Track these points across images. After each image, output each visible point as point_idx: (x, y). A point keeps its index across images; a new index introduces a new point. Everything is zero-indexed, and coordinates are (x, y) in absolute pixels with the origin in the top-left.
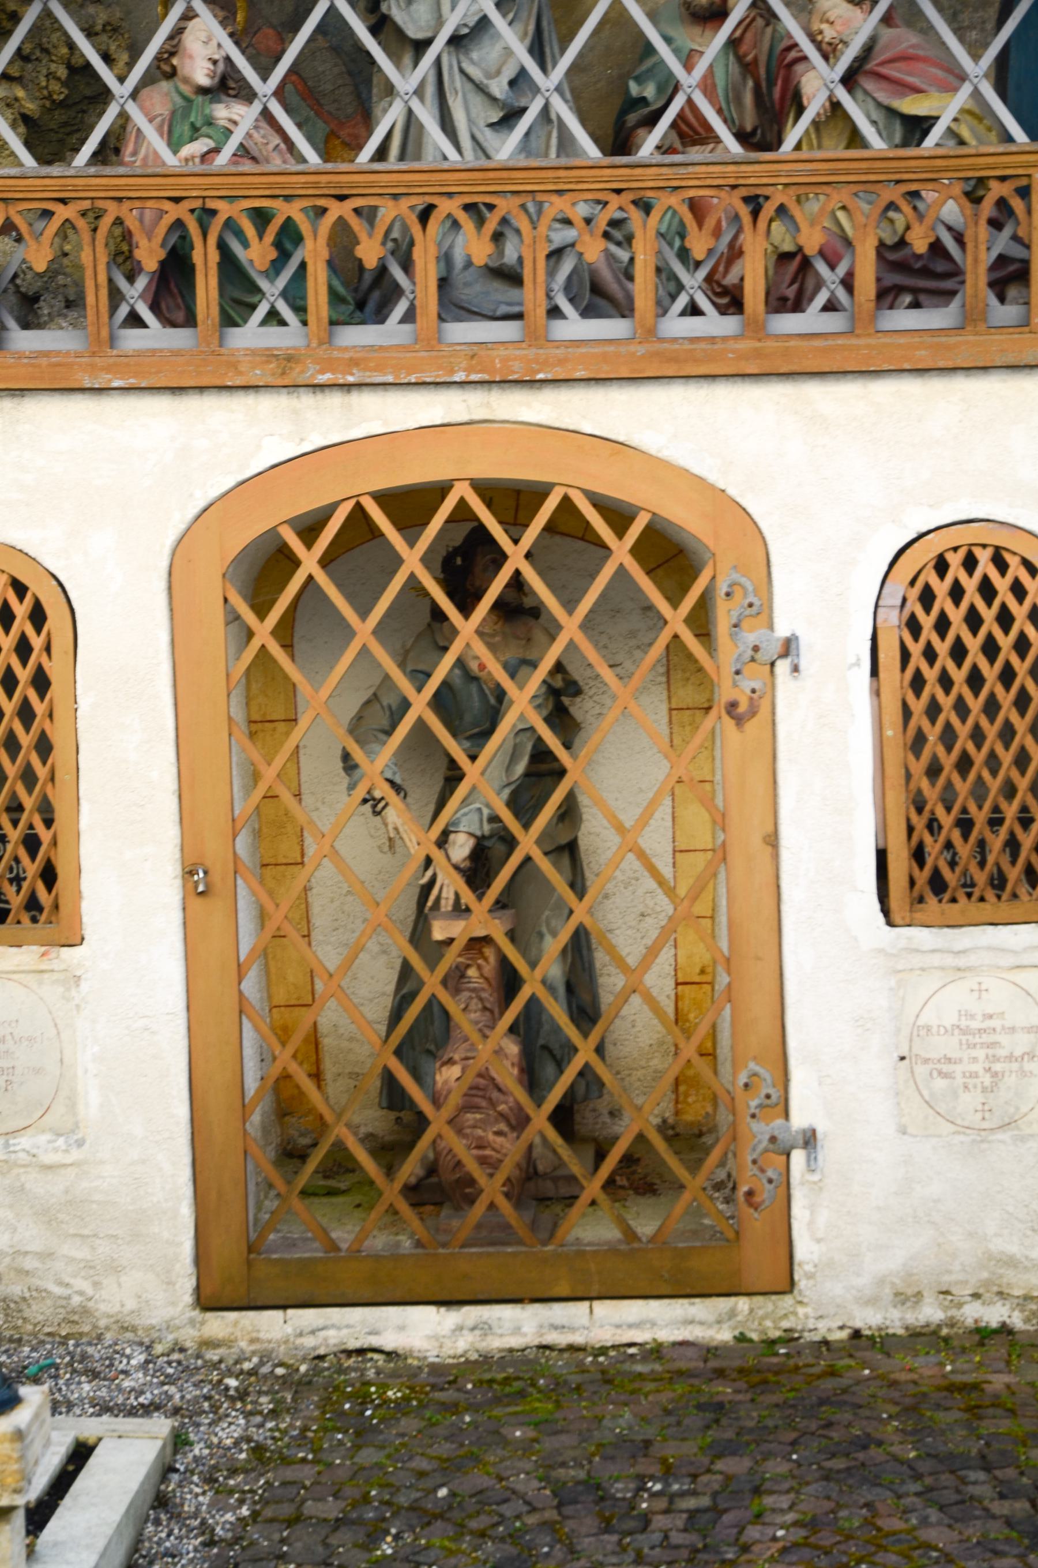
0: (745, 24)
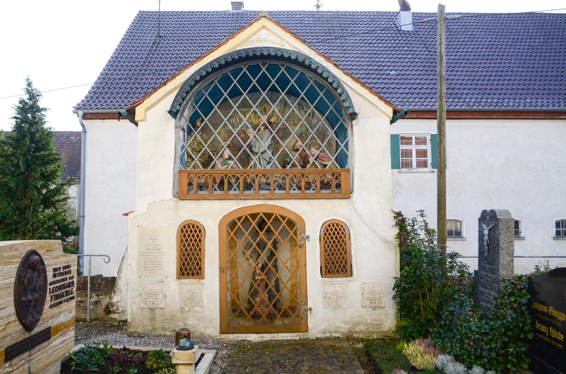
0: (301, 152)
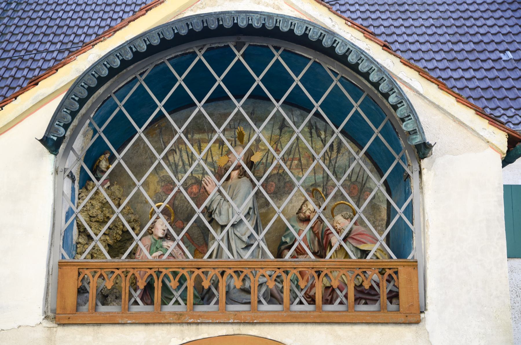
0: (316, 223)
